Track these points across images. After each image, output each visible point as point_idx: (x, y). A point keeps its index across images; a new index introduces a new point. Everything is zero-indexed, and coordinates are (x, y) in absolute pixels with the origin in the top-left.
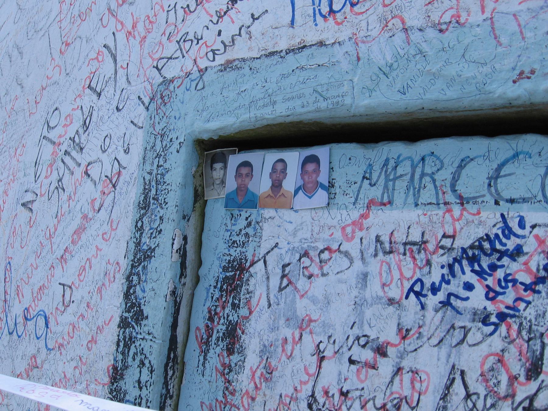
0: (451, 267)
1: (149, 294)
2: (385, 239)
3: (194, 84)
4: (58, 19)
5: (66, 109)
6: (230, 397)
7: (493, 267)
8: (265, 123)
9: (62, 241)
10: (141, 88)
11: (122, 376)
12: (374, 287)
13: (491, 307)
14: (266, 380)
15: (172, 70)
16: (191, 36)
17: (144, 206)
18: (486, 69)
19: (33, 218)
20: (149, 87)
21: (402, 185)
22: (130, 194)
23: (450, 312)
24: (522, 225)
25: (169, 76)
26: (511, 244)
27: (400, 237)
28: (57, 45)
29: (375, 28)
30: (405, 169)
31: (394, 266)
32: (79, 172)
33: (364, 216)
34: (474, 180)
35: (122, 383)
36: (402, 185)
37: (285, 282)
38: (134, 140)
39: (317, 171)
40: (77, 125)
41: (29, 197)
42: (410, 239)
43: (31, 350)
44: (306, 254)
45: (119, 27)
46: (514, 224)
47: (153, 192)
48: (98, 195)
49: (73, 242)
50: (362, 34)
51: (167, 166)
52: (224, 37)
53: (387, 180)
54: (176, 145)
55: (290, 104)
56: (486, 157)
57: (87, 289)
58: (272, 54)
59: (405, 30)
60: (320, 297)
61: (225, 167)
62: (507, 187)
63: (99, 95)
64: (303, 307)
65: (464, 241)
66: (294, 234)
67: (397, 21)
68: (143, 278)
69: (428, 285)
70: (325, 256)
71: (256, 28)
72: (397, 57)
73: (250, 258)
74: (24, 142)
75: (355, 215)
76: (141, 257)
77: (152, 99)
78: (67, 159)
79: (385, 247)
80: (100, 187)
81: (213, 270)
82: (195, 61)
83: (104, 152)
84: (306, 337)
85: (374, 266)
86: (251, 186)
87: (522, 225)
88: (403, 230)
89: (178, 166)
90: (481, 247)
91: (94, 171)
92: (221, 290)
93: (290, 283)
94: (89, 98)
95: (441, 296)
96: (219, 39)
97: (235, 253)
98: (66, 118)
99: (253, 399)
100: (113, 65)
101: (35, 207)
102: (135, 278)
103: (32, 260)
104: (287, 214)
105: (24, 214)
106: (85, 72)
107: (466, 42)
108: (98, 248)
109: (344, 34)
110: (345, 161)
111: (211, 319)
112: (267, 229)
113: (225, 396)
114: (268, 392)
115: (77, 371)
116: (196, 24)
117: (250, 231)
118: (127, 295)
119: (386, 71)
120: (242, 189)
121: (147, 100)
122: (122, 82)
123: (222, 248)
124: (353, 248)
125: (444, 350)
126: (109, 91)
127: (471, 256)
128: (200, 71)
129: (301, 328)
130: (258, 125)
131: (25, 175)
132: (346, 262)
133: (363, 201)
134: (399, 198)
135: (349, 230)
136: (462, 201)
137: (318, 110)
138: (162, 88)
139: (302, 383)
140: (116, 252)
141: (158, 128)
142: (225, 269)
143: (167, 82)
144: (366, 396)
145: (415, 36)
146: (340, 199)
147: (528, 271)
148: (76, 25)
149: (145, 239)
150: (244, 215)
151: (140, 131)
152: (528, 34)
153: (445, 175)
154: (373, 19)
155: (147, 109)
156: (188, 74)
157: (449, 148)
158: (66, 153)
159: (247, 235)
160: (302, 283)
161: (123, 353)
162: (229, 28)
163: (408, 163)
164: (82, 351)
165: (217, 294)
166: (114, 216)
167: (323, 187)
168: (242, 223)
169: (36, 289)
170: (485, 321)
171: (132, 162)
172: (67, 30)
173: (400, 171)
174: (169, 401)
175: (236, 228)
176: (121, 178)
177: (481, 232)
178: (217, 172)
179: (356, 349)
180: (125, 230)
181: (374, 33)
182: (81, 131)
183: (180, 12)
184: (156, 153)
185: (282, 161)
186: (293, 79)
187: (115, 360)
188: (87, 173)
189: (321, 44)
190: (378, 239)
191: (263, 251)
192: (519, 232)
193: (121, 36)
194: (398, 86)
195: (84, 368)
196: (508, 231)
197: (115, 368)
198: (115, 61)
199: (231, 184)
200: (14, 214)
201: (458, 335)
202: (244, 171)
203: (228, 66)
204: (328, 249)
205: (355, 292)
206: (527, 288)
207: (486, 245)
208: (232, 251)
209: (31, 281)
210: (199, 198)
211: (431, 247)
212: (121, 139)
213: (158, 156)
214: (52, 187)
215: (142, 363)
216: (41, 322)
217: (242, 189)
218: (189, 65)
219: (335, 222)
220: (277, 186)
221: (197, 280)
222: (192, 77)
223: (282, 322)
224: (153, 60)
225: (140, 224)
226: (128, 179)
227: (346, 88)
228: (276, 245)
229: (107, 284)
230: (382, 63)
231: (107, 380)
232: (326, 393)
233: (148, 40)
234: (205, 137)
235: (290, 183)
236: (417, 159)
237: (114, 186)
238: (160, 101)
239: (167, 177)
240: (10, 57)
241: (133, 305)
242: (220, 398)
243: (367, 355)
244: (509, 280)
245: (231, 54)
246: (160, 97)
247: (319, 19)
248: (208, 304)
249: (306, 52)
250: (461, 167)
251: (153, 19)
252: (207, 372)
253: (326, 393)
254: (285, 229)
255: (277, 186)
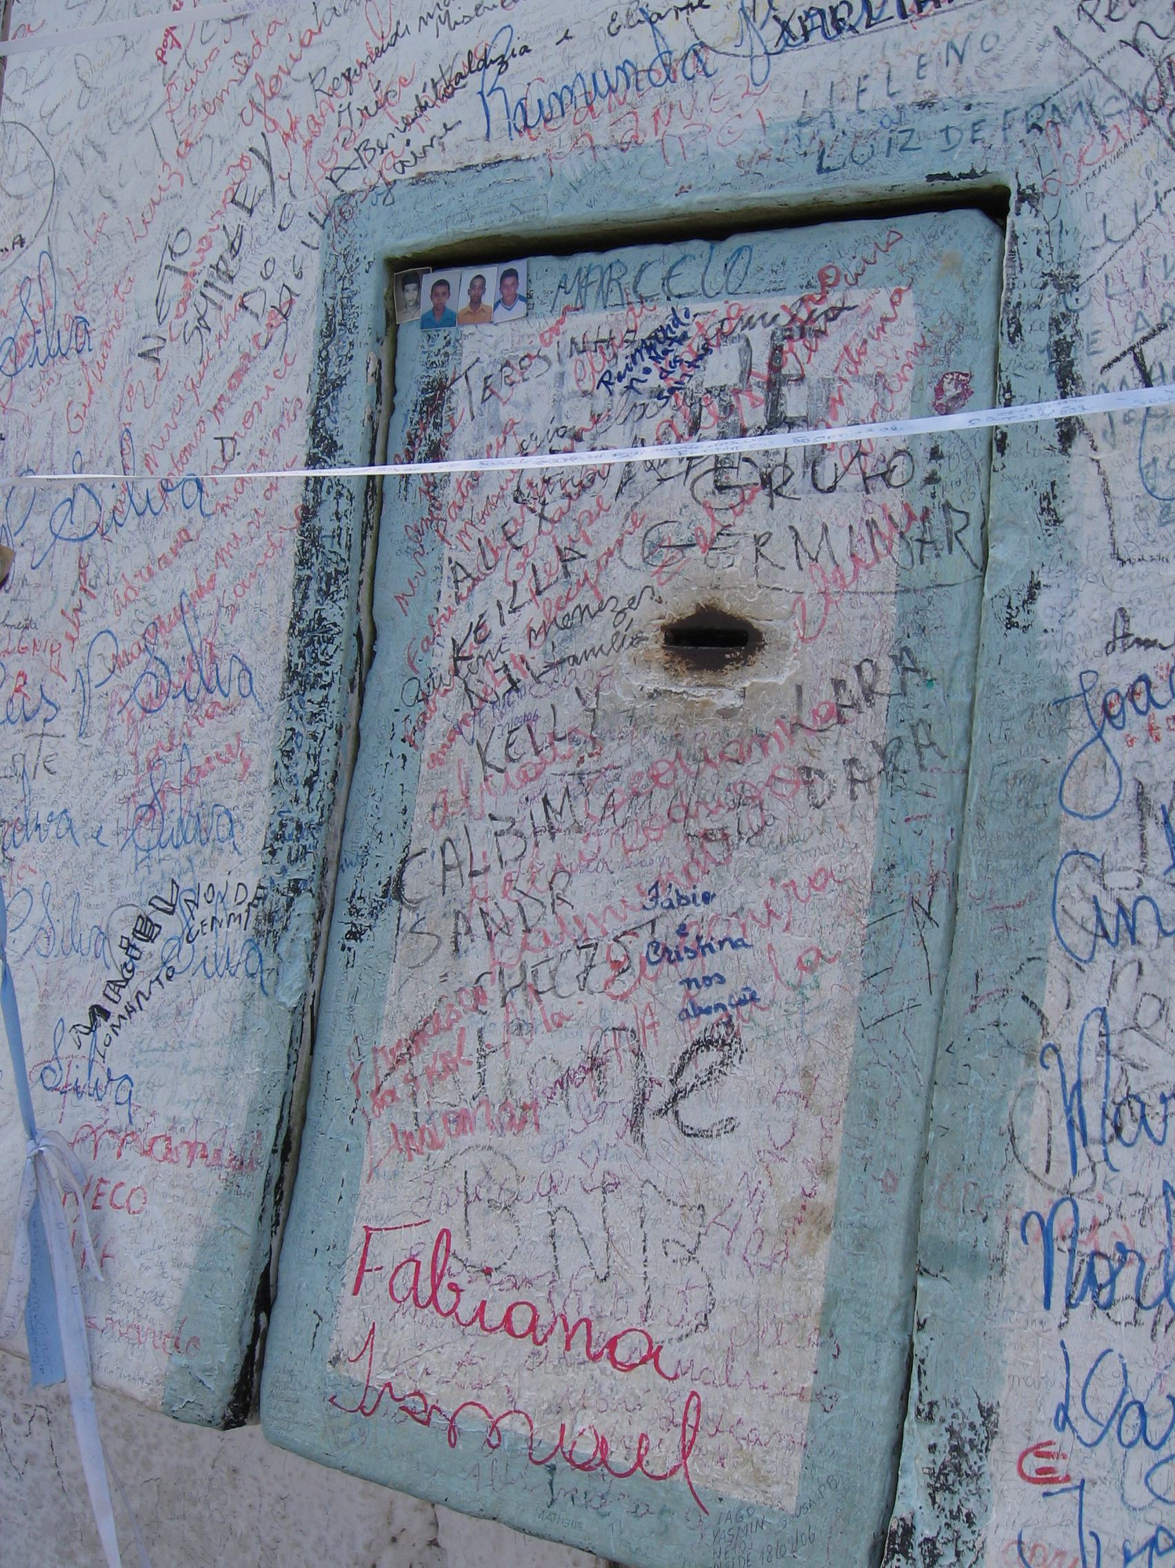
0: (633, 356)
1: (342, 423)
2: (579, 340)
3: (381, 199)
4: (166, 108)
5: (199, 229)
6: (436, 513)
7: (666, 352)
8: (463, 237)
9: (211, 391)
10: (307, 201)
11: (315, 514)
12: (571, 384)
13: (663, 384)
14: (473, 487)
15: (351, 183)
16: (373, 144)
17: (329, 333)
18: (656, 185)
19: (162, 370)
20: (322, 202)
21: (592, 291)
22: (307, 324)
23: (632, 393)
24: (687, 316)
25: (348, 189)
26: (678, 332)
27: (592, 337)
28: (170, 145)
29: (567, 144)
30: (595, 276)
31: (587, 363)
32: (230, 306)
33: (560, 322)
34: (651, 282)
35: (315, 522)
36: (592, 291)
37: (488, 393)
38: (307, 263)
39: (516, 284)
40: (219, 248)
41: (151, 344)
42: (602, 337)
43: (180, 523)
44: (507, 364)
45: (271, 126)
46: (681, 316)
47: (339, 317)
48: (262, 329)
49: (230, 387)
50: (555, 150)
51: (354, 288)
52: (413, 146)
53: (580, 287)
54: (364, 265)
55: (488, 218)
56: (661, 261)
57: (259, 435)
58: (468, 167)
59: (593, 148)
60: (522, 401)
61: (419, 287)
62: (677, 286)
63: (251, 211)
64: (505, 413)
65: (643, 334)
66: (495, 347)
67: (586, 139)
68: (333, 409)
69: (615, 374)
70: (526, 363)
71: (449, 139)
72: (586, 173)
73: (450, 376)
74: (129, 274)
75: (552, 322)
76: (328, 388)
77: (328, 216)
78: (209, 292)
79: (579, 348)
80: (265, 321)
81: (410, 393)
82: (381, 173)
83: (267, 278)
84: (510, 440)
85: (570, 365)
86: (449, 304)
87: (687, 316)
88: (594, 329)
89: (368, 288)
90: (656, 337)
91: (254, 303)
92: (421, 412)
93: (493, 393)
94: (234, 217)
95: (625, 382)
96: (408, 149)
97: (434, 373)
98: (200, 241)
99: (461, 508)
100: (267, 174)
101: (162, 355)
102: (323, 411)
103: (167, 418)
104: (487, 329)
105: (148, 366)
106: (224, 182)
107: (642, 160)
108: (268, 389)
109: (538, 150)
110: (542, 272)
111: (411, 443)
112: (468, 346)
113: (431, 513)
114: (475, 498)
115: (253, 527)
116: (379, 129)
117: (450, 350)
118: (314, 431)
119: (575, 187)
120: (439, 309)
121: (321, 217)
122: (283, 195)
123: (420, 371)
124: (551, 352)
125: (629, 425)
126: (265, 206)
127: (648, 346)
128: (387, 184)
129: (505, 432)
130: (457, 239)
131: (139, 317)
132: (545, 366)
133: (559, 308)
134: (590, 302)
135: (547, 336)
136: (642, 300)
137: (515, 224)
138: (340, 202)
139: (507, 481)
140: (298, 386)
141: (339, 248)
142: (424, 391)
143: (346, 196)
144: (566, 478)
145: (602, 154)
146: (538, 309)
147: (691, 351)
148: (199, 119)
149: (333, 368)
150: (442, 334)
151: (315, 253)
152: (689, 155)
153: (628, 279)
154: (565, 136)
155: (323, 226)
156: (373, 188)
157: (631, 255)
158: (207, 284)
159: (446, 354)
160: (504, 392)
161: (314, 491)
162: (419, 138)
163: (598, 271)
164: (259, 503)
165: (417, 418)
166: (288, 350)
167: (521, 298)
168: (440, 343)
169: (177, 454)
170: (659, 397)
171: (308, 289)
172: (185, 125)
173: (591, 279)
174: (369, 533)
175: (435, 349)
176: (295, 307)
177: (656, 325)
178: (410, 293)
179: (556, 440)
180: (305, 362)
181: (566, 150)
182: (227, 256)
183: (357, 116)
184: (339, 274)
185: (480, 276)
186: (490, 193)
187: (305, 500)
188: (242, 306)
189: (517, 159)
190: (573, 341)
191: (464, 367)
192: (685, 321)
193: (275, 140)
194: (586, 200)
195: (262, 520)
196: (677, 322)
197: (305, 509)
198: (270, 169)
199: (427, 305)
200: (126, 368)
201: (639, 411)
202: (441, 290)
203: (420, 179)
204: (528, 356)
205: (553, 391)
206: (691, 364)
207: (661, 335)
208: (431, 373)
209: (169, 445)
210: (391, 324)
211: (617, 342)
212: (289, 262)
213: (342, 278)
214: (189, 329)
215: (340, 494)
216: (192, 488)
217: (439, 309)
218: (373, 177)
219: (533, 331)
220: (476, 302)
221: (392, 408)
222: (379, 190)
223: (486, 431)
224: (325, 170)
225: (324, 354)
226: (303, 306)
227: (541, 202)
228: (478, 360)
229: (286, 423)
230: (573, 178)
231: (295, 523)
232: (530, 484)
233: (315, 146)
234: (398, 255)
235: (488, 299)
236: (606, 266)
237: (285, 317)
238: (338, 218)
239: (354, 301)
240: (80, 158)
241: (323, 439)
242: (427, 516)
243: (566, 442)
244: (678, 361)
245: (422, 167)
246: (339, 213)
247: (515, 134)
248: (408, 429)
249: (502, 166)
250: (641, 271)
251: (320, 121)
252: (410, 495)
253: (530, 484)
254: (483, 344)
255: (476, 302)
